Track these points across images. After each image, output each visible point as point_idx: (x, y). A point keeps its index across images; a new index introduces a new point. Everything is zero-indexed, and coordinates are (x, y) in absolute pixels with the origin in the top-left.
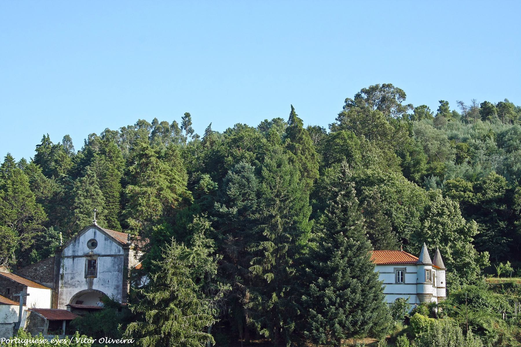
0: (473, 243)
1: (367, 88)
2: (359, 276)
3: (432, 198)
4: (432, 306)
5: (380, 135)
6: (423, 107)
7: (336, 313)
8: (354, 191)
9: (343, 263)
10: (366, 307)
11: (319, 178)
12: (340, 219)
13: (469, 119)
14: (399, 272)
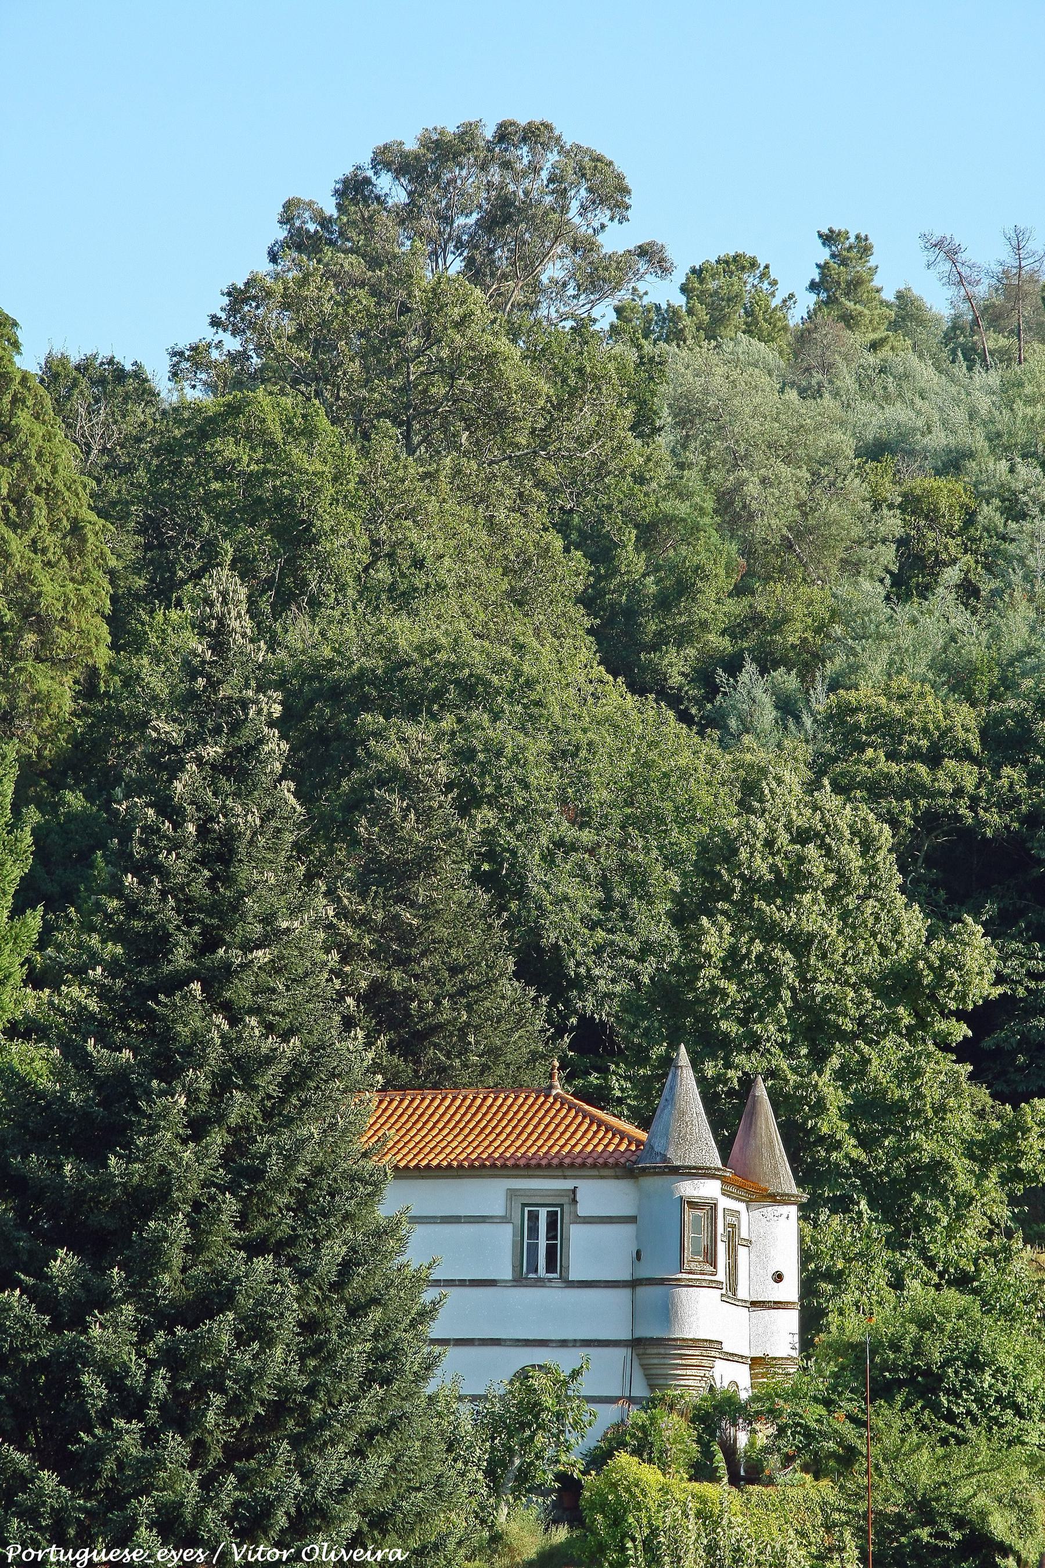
0: (963, 1052)
1: (411, 145)
2: (292, 1240)
3: (750, 792)
4: (715, 1414)
5: (469, 424)
6: (737, 264)
7: (142, 1461)
8: (276, 747)
9: (194, 1164)
10: (323, 1424)
11: (112, 669)
12: (187, 906)
13: (993, 341)
14: (534, 1217)
